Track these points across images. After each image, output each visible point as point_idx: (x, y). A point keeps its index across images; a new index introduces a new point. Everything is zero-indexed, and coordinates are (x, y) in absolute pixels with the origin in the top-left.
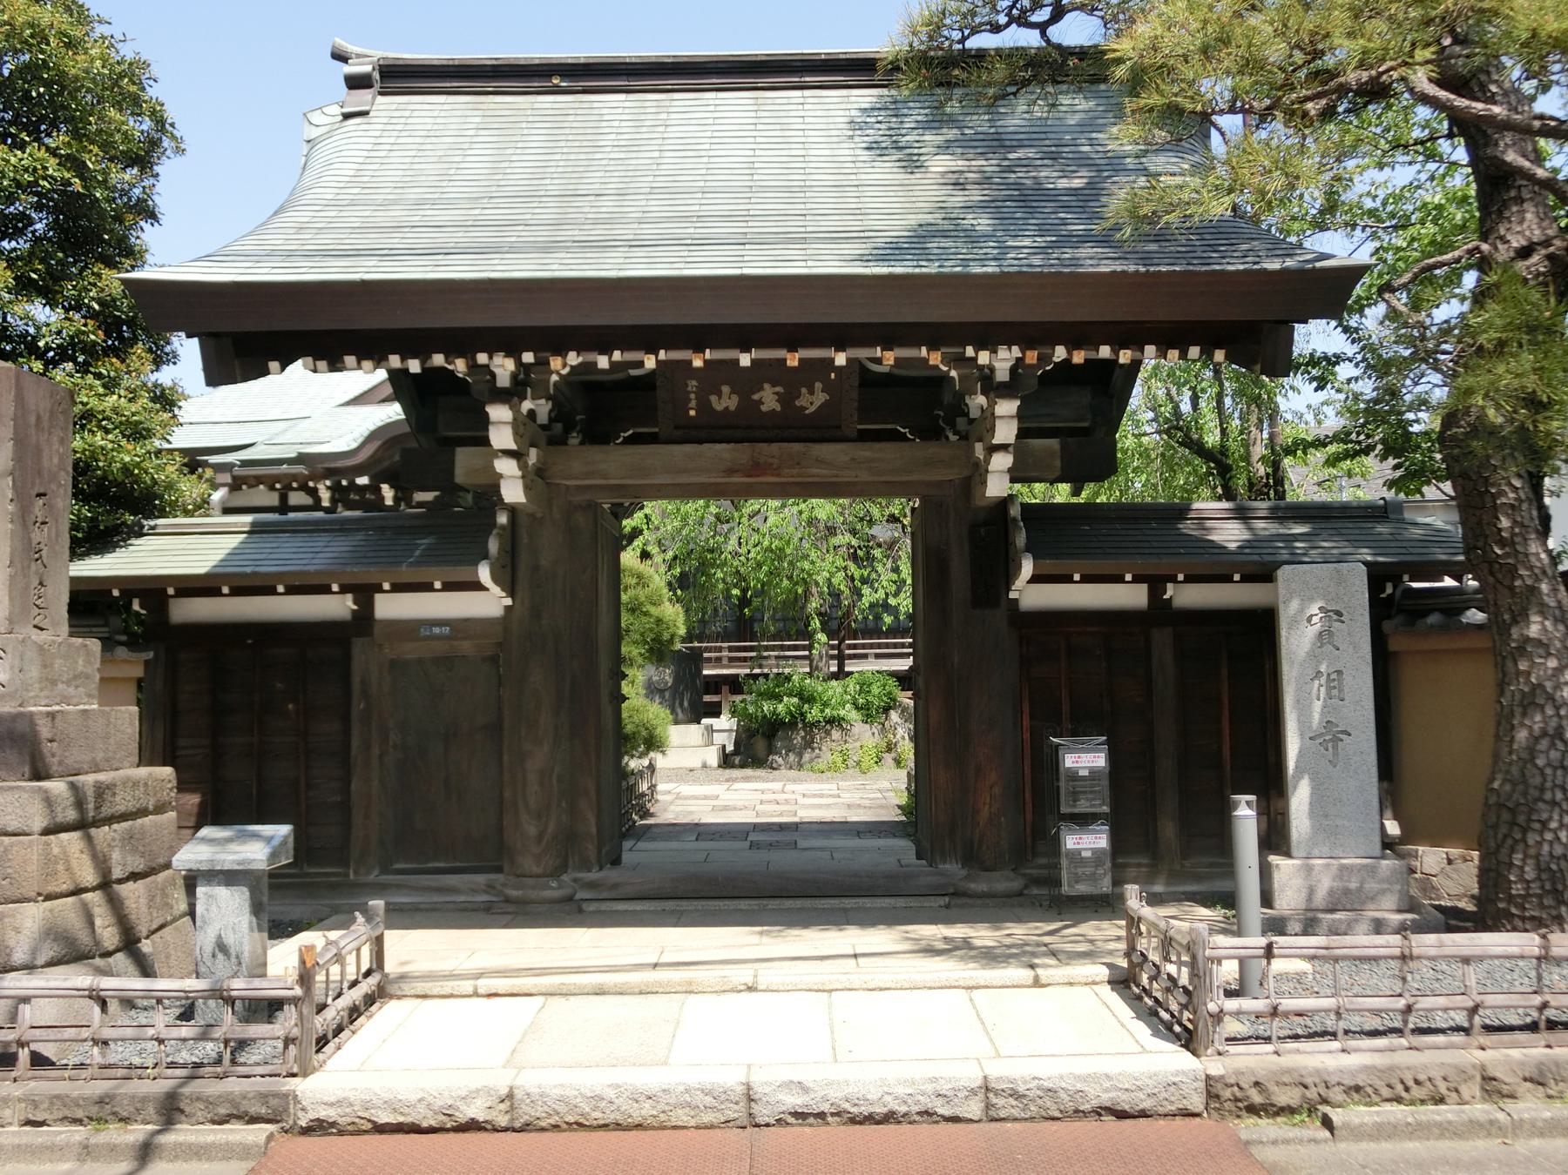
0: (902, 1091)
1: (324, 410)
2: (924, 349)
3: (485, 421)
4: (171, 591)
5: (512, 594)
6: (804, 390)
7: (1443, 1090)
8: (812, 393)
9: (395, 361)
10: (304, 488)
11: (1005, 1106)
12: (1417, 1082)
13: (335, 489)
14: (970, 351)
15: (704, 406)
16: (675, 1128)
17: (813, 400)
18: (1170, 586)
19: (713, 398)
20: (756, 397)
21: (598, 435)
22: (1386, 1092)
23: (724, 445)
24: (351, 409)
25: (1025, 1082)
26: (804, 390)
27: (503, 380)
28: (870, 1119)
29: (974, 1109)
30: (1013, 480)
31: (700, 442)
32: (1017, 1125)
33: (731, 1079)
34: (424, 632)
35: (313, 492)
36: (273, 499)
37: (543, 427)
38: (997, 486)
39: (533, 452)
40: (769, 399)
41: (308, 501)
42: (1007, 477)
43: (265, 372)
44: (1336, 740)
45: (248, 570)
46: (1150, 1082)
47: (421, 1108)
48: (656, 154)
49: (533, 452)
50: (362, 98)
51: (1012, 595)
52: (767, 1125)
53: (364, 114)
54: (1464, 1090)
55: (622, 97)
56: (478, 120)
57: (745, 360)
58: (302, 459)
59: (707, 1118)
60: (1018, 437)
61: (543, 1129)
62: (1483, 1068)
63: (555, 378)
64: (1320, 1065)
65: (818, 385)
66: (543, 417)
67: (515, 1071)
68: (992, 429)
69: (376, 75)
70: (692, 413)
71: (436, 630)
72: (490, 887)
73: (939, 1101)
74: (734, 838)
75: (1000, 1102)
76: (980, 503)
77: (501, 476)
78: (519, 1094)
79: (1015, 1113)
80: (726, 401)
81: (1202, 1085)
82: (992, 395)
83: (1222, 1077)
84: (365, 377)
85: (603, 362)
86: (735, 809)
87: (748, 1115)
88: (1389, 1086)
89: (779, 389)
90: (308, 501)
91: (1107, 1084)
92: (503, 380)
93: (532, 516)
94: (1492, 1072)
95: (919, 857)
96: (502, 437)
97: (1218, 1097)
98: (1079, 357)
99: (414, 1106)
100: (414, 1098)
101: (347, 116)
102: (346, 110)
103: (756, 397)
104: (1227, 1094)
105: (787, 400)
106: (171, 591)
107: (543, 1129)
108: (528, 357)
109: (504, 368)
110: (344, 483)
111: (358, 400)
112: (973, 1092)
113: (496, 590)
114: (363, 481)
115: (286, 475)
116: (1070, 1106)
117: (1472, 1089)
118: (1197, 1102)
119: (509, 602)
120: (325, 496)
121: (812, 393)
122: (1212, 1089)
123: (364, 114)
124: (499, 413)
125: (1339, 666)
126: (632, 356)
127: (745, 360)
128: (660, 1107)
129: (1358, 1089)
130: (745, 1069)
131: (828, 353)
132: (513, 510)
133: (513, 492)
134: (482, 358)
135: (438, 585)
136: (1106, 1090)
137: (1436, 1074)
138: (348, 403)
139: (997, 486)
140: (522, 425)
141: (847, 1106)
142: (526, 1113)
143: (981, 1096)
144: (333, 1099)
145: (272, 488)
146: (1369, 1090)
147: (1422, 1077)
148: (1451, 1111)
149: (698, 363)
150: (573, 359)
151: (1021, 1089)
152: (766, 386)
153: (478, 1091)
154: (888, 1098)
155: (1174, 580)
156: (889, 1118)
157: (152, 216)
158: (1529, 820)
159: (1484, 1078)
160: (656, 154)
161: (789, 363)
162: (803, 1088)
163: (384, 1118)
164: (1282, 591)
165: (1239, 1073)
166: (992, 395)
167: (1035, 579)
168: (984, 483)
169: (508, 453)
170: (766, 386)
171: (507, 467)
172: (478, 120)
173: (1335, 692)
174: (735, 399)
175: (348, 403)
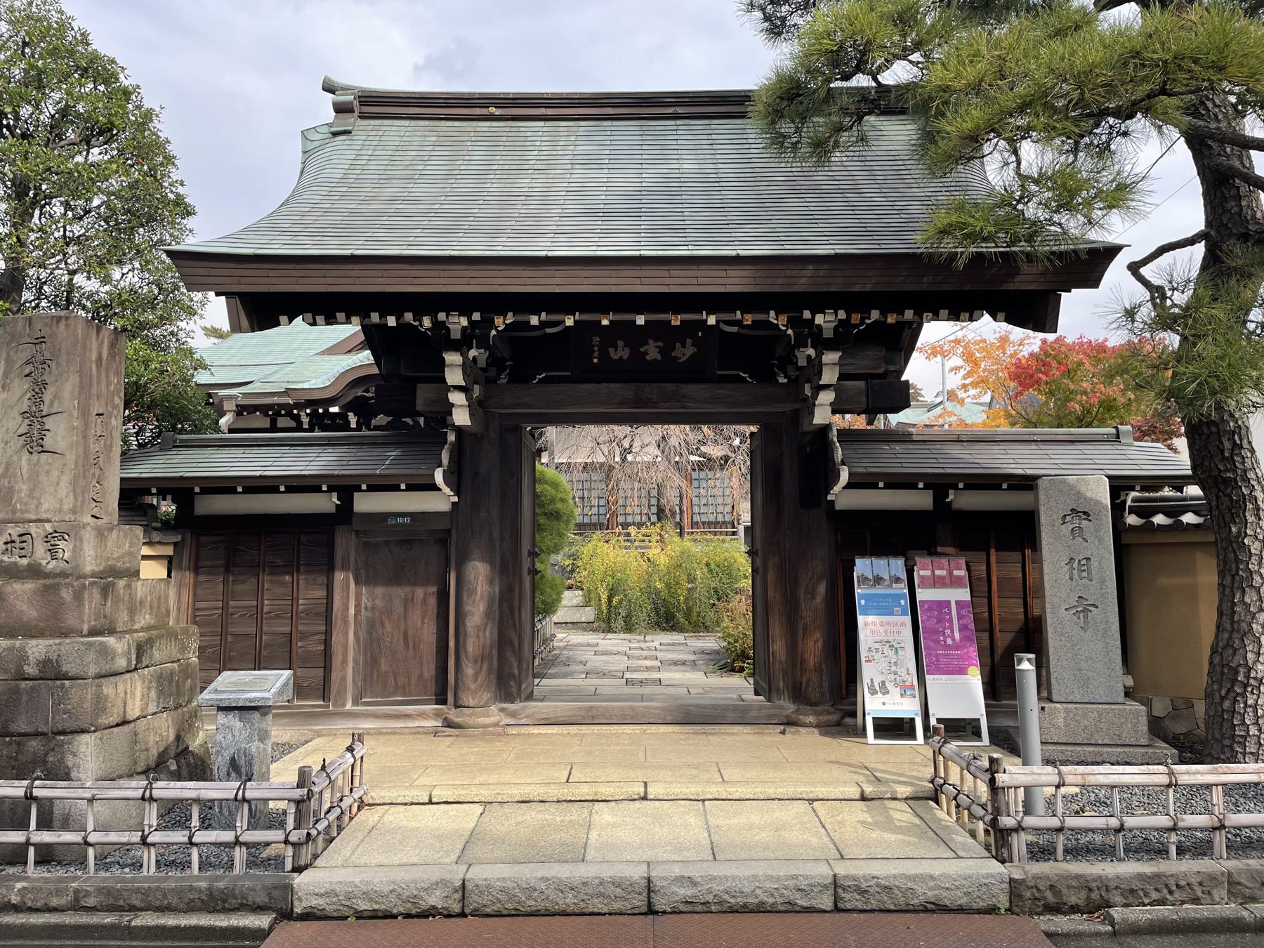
0: (770, 885)
1: (315, 356)
2: (738, 313)
3: (442, 365)
4: (197, 490)
5: (458, 493)
6: (678, 345)
7: (1199, 894)
8: (684, 346)
9: (375, 317)
10: (289, 414)
11: (851, 900)
12: (1178, 886)
13: (314, 415)
14: (807, 314)
15: (604, 356)
16: (591, 914)
17: (684, 352)
18: (951, 492)
19: (611, 351)
20: (642, 349)
21: (520, 377)
22: (1155, 895)
23: (617, 385)
24: (326, 357)
25: (866, 881)
26: (678, 345)
27: (456, 334)
28: (745, 909)
29: (826, 902)
30: (834, 412)
31: (599, 382)
32: (862, 916)
33: (637, 873)
34: (391, 521)
35: (297, 418)
36: (266, 423)
37: (481, 369)
38: (822, 415)
39: (477, 388)
40: (652, 351)
41: (293, 424)
42: (829, 409)
43: (277, 324)
44: (1085, 611)
45: (258, 474)
46: (965, 883)
47: (393, 898)
48: (569, 167)
49: (477, 388)
50: (350, 121)
51: (830, 498)
52: (664, 912)
53: (349, 132)
54: (1215, 892)
55: (541, 124)
56: (434, 139)
57: (640, 320)
58: (287, 392)
59: (617, 906)
60: (839, 379)
61: (488, 915)
62: (1230, 874)
63: (493, 332)
64: (1102, 872)
65: (689, 341)
66: (482, 363)
67: (465, 867)
68: (820, 374)
69: (356, 103)
70: (595, 361)
71: (401, 520)
72: (437, 715)
73: (798, 895)
74: (614, 677)
75: (847, 896)
76: (806, 428)
77: (453, 405)
78: (469, 886)
79: (860, 906)
80: (620, 352)
81: (1006, 886)
82: (819, 348)
83: (1024, 880)
84: (350, 330)
85: (534, 320)
86: (611, 654)
87: (649, 905)
88: (1156, 890)
89: (660, 344)
90: (293, 424)
91: (931, 884)
92: (456, 334)
93: (474, 435)
94: (1236, 877)
95: (757, 693)
96: (454, 377)
97: (1020, 896)
98: (891, 319)
99: (387, 896)
100: (386, 889)
101: (335, 134)
102: (334, 129)
103: (642, 349)
104: (1028, 894)
105: (666, 351)
106: (197, 490)
107: (488, 915)
108: (476, 316)
109: (458, 323)
110: (321, 411)
111: (331, 351)
112: (825, 887)
113: (447, 490)
114: (334, 409)
115: (278, 405)
116: (902, 901)
117: (1220, 893)
118: (1003, 902)
119: (455, 499)
120: (305, 421)
121: (684, 346)
122: (1014, 886)
123: (349, 132)
124: (452, 358)
125: (1088, 554)
126: (521, 318)
127: (640, 320)
128: (582, 896)
129: (1132, 891)
130: (645, 867)
131: (670, 316)
132: (459, 430)
133: (461, 417)
134: (442, 316)
135: (403, 486)
136: (931, 889)
137: (1194, 880)
138: (323, 353)
139: (822, 415)
140: (468, 367)
141: (726, 897)
142: (474, 901)
143: (831, 891)
144: (322, 891)
145: (266, 415)
146: (1141, 893)
147: (1183, 883)
148: (1208, 910)
149: (605, 322)
150: (510, 318)
151: (864, 885)
152: (651, 341)
153: (437, 883)
154: (758, 892)
155: (955, 487)
156: (760, 909)
157: (188, 212)
158: (1248, 677)
159: (1229, 883)
160: (569, 167)
161: (673, 323)
162: (692, 882)
163: (363, 906)
164: (1042, 497)
165: (1035, 877)
166: (819, 348)
167: (849, 486)
168: (812, 414)
169: (458, 388)
170: (651, 341)
171: (457, 398)
172: (434, 139)
173: (1085, 574)
174: (627, 351)
175: (323, 353)
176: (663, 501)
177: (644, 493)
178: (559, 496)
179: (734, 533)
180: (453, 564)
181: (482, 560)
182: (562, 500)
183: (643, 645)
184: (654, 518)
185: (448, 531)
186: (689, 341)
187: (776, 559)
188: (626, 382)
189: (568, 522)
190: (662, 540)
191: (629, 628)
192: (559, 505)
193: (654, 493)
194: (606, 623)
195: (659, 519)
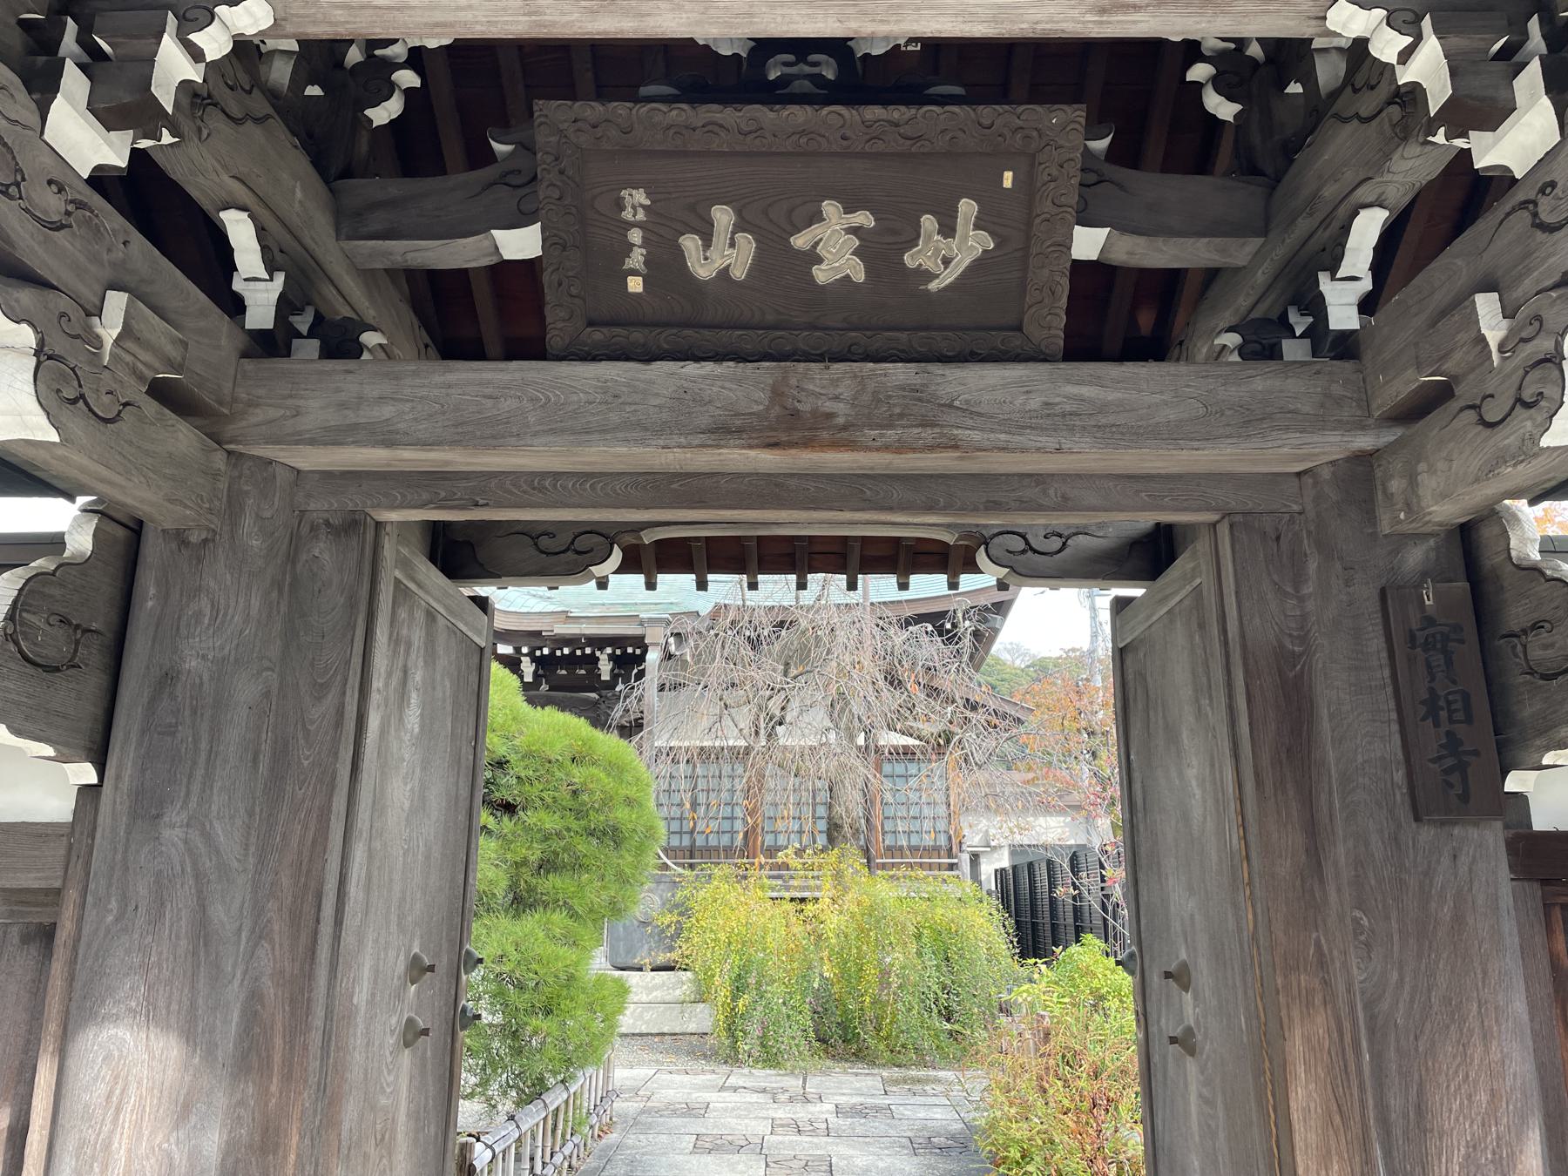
6: (928, 222)
8: (948, 230)
19: (690, 244)
20: (800, 241)
26: (928, 222)
65: (967, 208)
89: (864, 219)
103: (800, 241)
121: (948, 230)
152: (830, 208)
170: (830, 208)
176: (839, 810)
177: (806, 797)
178: (623, 792)
179: (951, 867)
180: (52, 1027)
181: (152, 1014)
182: (629, 802)
183: (801, 1113)
184: (821, 840)
185: (54, 896)
186: (967, 208)
187: (1320, 1023)
188: (741, 357)
189: (640, 850)
190: (838, 875)
191: (770, 1058)
192: (621, 814)
193: (823, 796)
194: (728, 1045)
195: (831, 840)
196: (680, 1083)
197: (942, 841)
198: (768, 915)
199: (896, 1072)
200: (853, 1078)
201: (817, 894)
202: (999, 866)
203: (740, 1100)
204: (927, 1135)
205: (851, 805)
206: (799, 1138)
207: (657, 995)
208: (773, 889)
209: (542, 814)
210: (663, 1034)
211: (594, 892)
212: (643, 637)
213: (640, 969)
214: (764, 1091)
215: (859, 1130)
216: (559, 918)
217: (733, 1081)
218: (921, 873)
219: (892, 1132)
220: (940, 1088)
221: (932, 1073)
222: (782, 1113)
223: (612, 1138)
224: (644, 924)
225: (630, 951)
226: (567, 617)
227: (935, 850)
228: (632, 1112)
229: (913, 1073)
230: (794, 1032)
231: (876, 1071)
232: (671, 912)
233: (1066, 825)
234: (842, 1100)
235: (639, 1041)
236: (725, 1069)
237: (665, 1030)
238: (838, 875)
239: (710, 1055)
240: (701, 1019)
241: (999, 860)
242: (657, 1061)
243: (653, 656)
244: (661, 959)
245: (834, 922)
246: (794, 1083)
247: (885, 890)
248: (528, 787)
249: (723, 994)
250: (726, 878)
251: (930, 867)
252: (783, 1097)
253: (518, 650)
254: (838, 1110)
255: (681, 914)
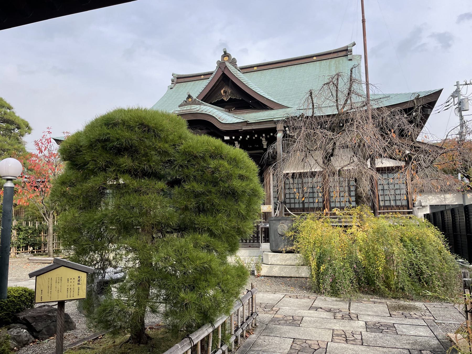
182: (242, 177)
190: (361, 217)
192: (237, 184)
195: (357, 203)
196: (293, 304)
197: (405, 203)
198: (331, 232)
199: (393, 302)
200: (373, 305)
201: (350, 224)
202: (425, 213)
203: (316, 318)
204: (419, 348)
205: (365, 187)
206: (345, 345)
207: (289, 262)
208: (332, 222)
209: (195, 184)
210: (291, 277)
211: (223, 222)
212: (275, 128)
213: (281, 252)
214: (330, 311)
215: (380, 343)
216: (204, 238)
217: (318, 303)
218: (400, 215)
219: (398, 345)
220: (419, 314)
221: (412, 303)
222: (339, 326)
223: (253, 337)
224: (282, 236)
225: (277, 245)
226: (247, 123)
227: (402, 206)
228: (267, 320)
229: (402, 302)
230: (345, 284)
231: (383, 301)
232: (291, 231)
233: (454, 197)
234: (369, 319)
235: (281, 280)
236: (313, 296)
237: (292, 276)
238: (361, 217)
239: (309, 289)
240: (304, 272)
241: (426, 211)
242: (286, 290)
243: (280, 135)
244: (289, 249)
245: (360, 235)
246: (344, 306)
247: (383, 222)
248: (186, 170)
249: (314, 264)
250: (313, 219)
251: (404, 213)
252: (339, 315)
253: (231, 138)
254: (367, 326)
255: (295, 232)
